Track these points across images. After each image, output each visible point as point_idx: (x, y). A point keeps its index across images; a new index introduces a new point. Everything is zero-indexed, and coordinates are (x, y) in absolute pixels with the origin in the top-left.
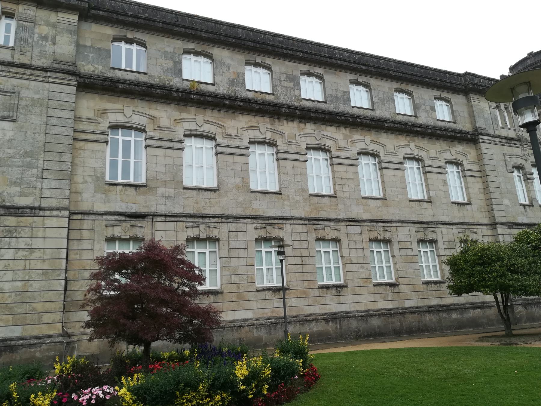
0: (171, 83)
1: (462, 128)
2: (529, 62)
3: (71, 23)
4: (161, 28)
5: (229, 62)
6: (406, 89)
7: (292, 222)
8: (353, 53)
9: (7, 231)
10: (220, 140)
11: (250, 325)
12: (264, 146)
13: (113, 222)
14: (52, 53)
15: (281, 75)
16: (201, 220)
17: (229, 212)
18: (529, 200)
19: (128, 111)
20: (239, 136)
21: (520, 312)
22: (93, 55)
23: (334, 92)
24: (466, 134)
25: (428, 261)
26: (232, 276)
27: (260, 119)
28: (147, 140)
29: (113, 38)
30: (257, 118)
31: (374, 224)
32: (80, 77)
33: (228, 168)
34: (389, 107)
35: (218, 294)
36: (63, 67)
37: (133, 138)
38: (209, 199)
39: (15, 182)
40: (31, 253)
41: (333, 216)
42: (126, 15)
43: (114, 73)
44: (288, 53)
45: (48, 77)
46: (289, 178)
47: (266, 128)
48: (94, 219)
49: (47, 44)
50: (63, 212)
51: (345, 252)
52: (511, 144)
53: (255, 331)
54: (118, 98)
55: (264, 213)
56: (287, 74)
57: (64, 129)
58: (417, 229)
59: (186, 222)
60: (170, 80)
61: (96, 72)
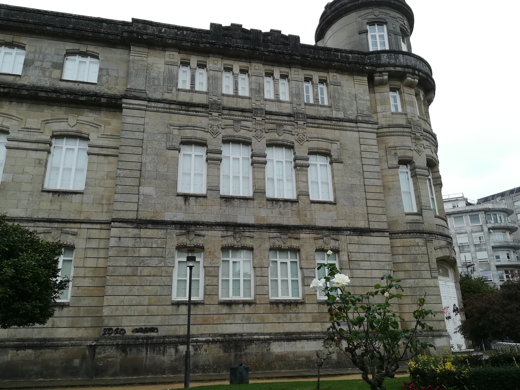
1: (106, 90)
10: (13, 134)
12: (76, 140)
24: (98, 97)
28: (208, 154)
52: (188, 111)
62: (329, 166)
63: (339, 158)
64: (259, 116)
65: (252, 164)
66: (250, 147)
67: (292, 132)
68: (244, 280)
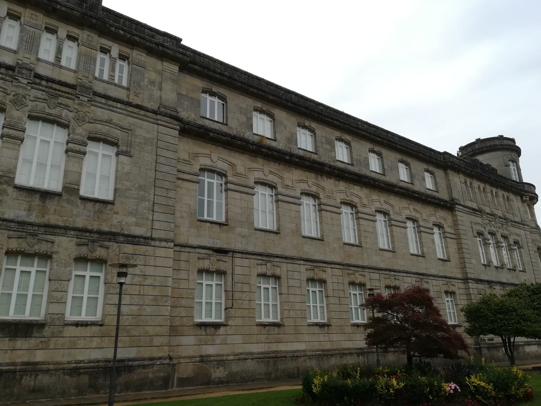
0: (245, 136)
1: (442, 197)
2: (477, 146)
3: (173, 73)
4: (240, 86)
6: (406, 161)
8: (370, 126)
9: (126, 258)
13: (204, 255)
14: (158, 98)
16: (268, 259)
18: (487, 261)
19: (215, 157)
21: (485, 354)
22: (187, 103)
25: (211, 297)
26: (291, 311)
27: (308, 174)
31: (388, 272)
32: (182, 123)
34: (395, 174)
36: (168, 112)
37: (216, 181)
38: (273, 240)
39: (132, 213)
41: (360, 263)
42: (215, 72)
47: (313, 182)
48: (189, 251)
49: (154, 88)
50: (169, 243)
51: (284, 290)
53: (308, 361)
54: (206, 144)
55: (312, 256)
56: (326, 138)
57: (170, 168)
58: (417, 279)
59: (257, 259)
60: (244, 133)
61: (190, 118)
62: (114, 158)
63: (129, 151)
64: (25, 77)
66: (4, 114)
67: (70, 108)
68: (216, 303)
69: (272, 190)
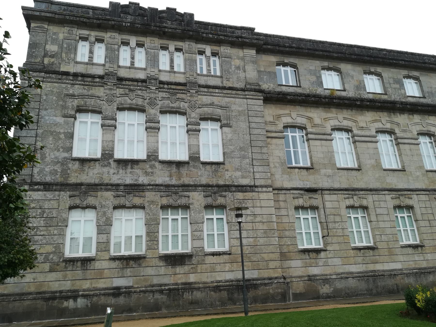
0: (317, 92)
3: (252, 56)
4: (307, 53)
5: (352, 73)
7: (417, 193)
8: (268, 36)
10: (309, 130)
11: (402, 274)
15: (389, 80)
16: (353, 193)
17: (371, 186)
19: (294, 115)
20: (368, 128)
23: (430, 90)
27: (381, 114)
29: (277, 64)
30: (378, 113)
32: (265, 93)
33: (364, 152)
35: (374, 249)
36: (253, 87)
37: (298, 134)
38: (356, 176)
39: (238, 169)
40: (255, 218)
42: (285, 47)
43: (281, 89)
44: (394, 63)
45: (246, 95)
46: (409, 158)
47: (386, 120)
48: (285, 193)
50: (269, 189)
53: (406, 278)
54: (285, 106)
55: (396, 186)
56: (394, 78)
59: (344, 194)
61: (270, 88)
65: (188, 131)
68: (172, 235)
69: (348, 134)
